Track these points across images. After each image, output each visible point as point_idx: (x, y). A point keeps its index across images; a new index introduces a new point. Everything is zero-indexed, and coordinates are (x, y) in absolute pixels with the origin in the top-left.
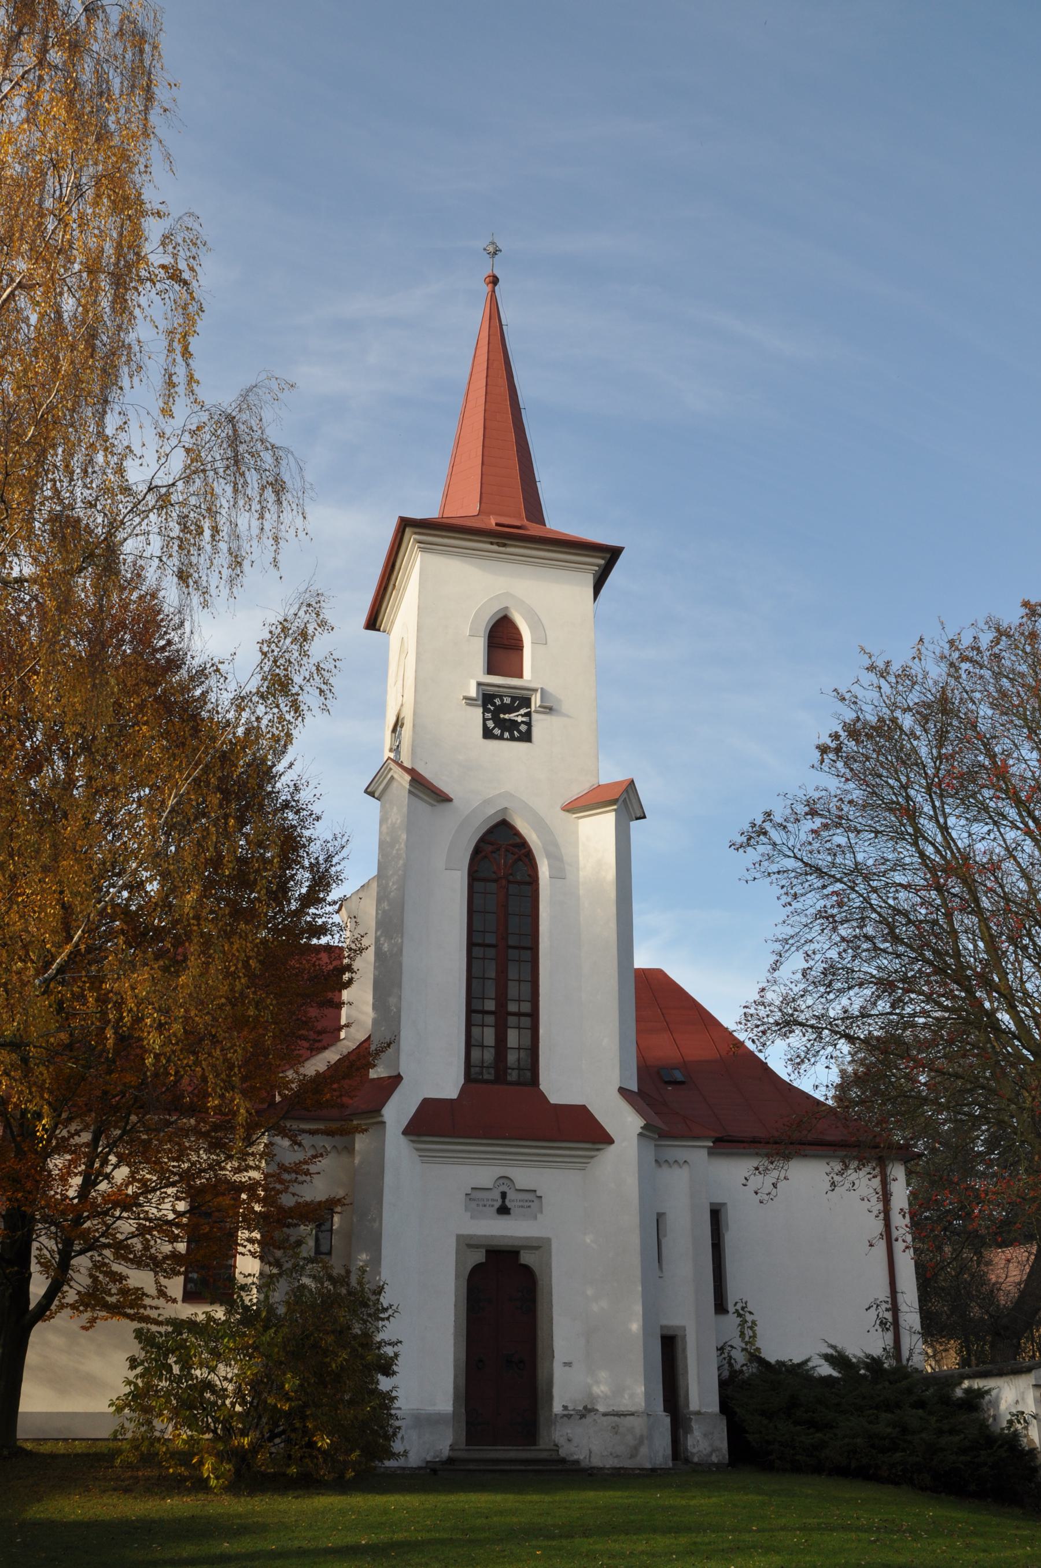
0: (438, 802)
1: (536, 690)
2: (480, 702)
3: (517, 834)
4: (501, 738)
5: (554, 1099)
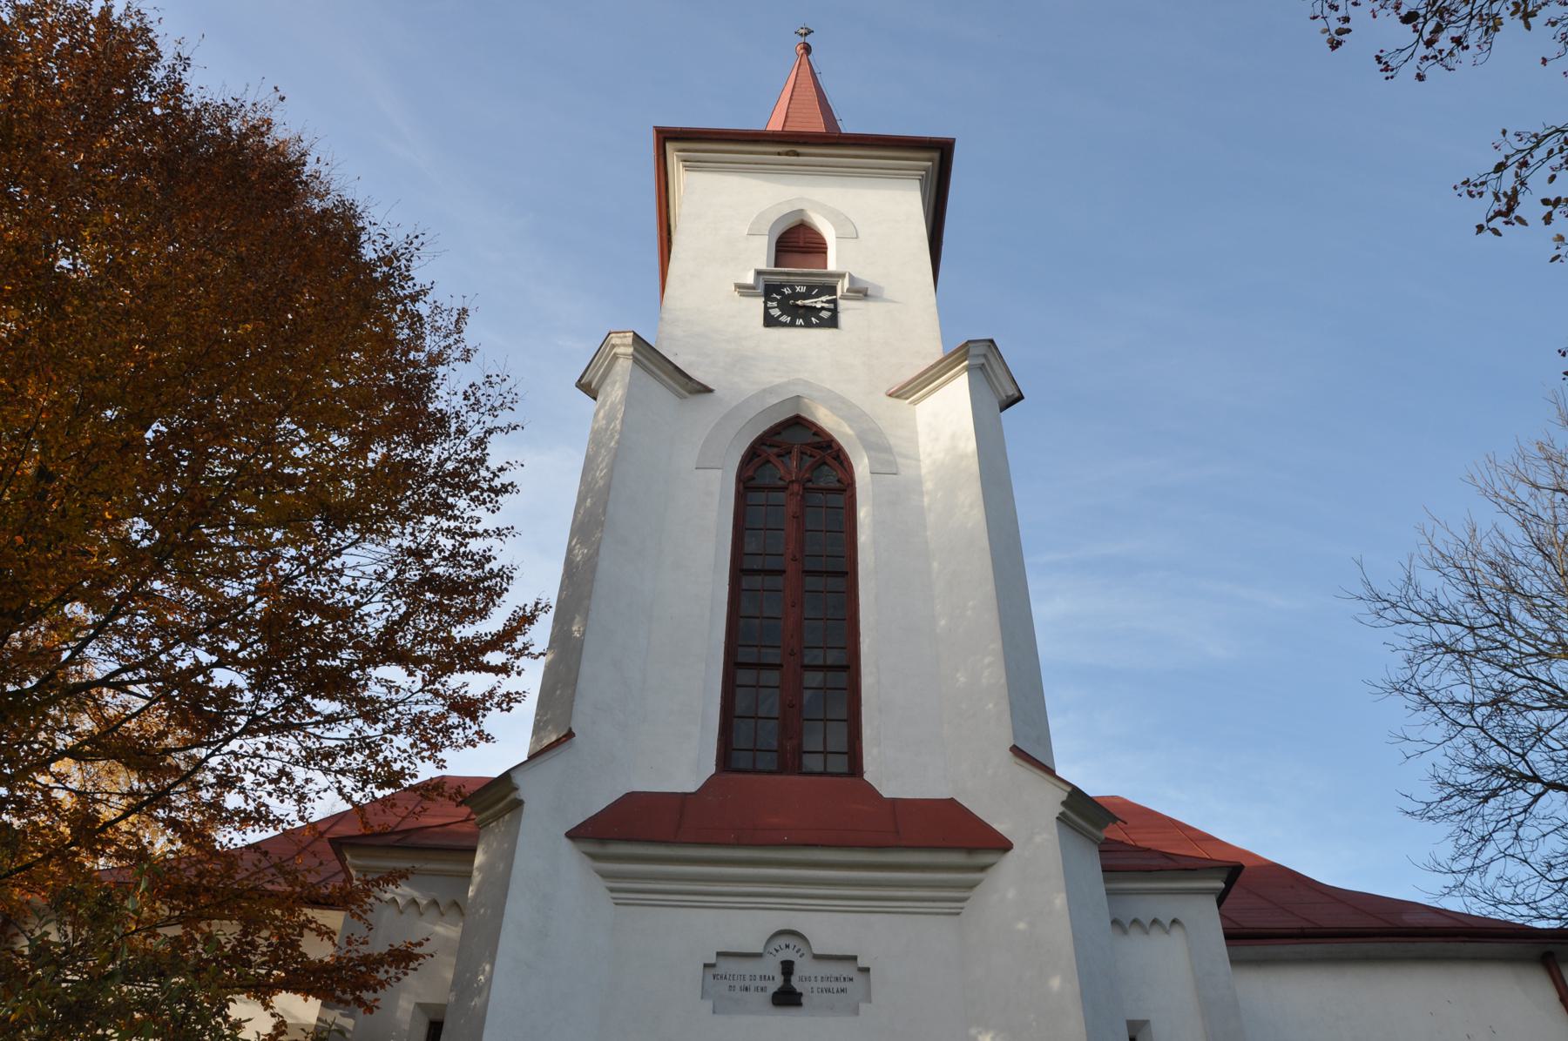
0: (690, 392)
1: (842, 276)
2: (760, 290)
3: (818, 431)
4: (792, 324)
5: (888, 790)
